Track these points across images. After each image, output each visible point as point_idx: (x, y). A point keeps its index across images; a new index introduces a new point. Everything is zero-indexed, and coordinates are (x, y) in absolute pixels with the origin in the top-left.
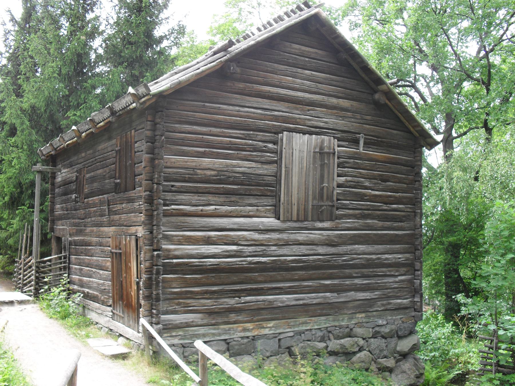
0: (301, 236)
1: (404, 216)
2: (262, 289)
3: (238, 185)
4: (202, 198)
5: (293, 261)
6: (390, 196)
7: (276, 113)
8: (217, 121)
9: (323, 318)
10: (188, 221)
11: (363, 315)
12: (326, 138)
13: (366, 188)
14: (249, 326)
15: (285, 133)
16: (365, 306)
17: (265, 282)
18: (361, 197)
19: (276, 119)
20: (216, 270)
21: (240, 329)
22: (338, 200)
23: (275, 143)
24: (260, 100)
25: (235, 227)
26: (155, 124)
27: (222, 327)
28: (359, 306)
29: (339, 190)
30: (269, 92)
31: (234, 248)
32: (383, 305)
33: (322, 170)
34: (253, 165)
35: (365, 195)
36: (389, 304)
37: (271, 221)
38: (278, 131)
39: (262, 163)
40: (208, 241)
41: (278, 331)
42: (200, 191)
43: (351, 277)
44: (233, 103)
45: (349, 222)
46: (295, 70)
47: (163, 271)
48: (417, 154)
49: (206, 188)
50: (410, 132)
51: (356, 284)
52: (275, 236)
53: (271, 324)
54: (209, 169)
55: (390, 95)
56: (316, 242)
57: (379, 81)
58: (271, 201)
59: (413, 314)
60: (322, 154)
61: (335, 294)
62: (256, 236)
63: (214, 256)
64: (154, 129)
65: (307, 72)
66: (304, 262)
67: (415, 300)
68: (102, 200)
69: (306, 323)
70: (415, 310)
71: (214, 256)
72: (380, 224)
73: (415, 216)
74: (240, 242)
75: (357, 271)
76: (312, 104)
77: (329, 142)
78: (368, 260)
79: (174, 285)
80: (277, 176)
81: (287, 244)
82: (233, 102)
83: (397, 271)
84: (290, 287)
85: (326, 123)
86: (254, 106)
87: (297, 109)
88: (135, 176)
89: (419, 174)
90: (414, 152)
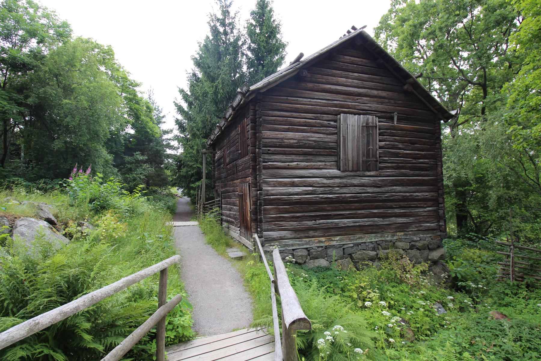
1: (429, 167)
2: (330, 215)
5: (350, 197)
7: (335, 102)
8: (296, 108)
9: (373, 235)
12: (370, 117)
13: (400, 149)
14: (323, 239)
15: (342, 114)
19: (336, 106)
20: (299, 203)
25: (311, 175)
29: (381, 151)
31: (311, 188)
32: (416, 227)
39: (327, 134)
40: (293, 185)
41: (342, 243)
45: (389, 171)
50: (431, 110)
51: (396, 213)
52: (337, 181)
53: (338, 238)
54: (292, 139)
61: (381, 219)
62: (325, 181)
65: (356, 74)
66: (358, 197)
67: (440, 224)
72: (412, 172)
73: (437, 167)
76: (360, 95)
78: (403, 196)
80: (338, 142)
81: (346, 186)
82: (306, 96)
84: (349, 214)
86: (321, 98)
87: (349, 99)
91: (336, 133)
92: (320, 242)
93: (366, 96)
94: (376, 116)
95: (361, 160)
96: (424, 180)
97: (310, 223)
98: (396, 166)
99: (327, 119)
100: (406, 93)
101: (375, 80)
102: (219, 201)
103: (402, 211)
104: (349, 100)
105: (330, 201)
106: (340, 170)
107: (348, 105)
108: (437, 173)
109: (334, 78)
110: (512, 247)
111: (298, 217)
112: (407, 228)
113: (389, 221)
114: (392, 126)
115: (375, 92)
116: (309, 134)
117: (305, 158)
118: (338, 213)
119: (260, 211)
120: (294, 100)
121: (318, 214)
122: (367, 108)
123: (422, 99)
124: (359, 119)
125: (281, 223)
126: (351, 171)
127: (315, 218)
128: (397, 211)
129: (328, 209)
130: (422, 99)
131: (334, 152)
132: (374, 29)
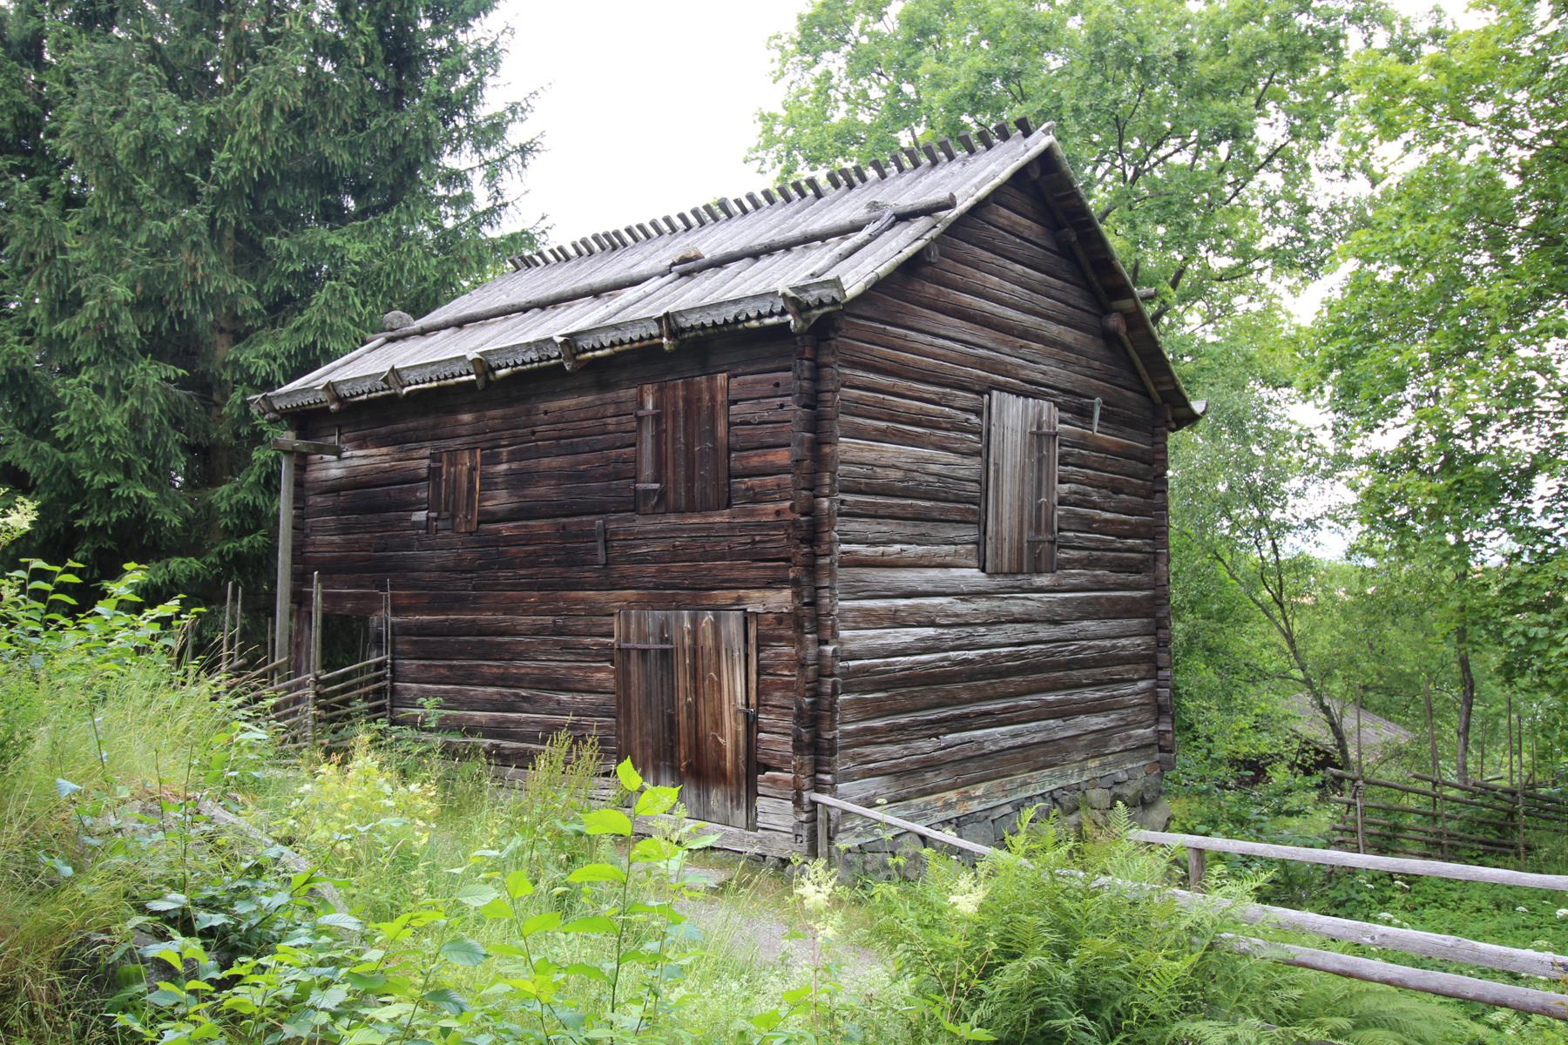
0: (1016, 606)
1: (1142, 562)
2: (966, 716)
3: (930, 500)
4: (884, 529)
5: (1009, 656)
6: (1125, 522)
7: (981, 352)
8: (903, 364)
9: (1047, 772)
10: (863, 577)
11: (1096, 763)
12: (1045, 404)
13: (1094, 506)
14: (952, 796)
15: (995, 393)
16: (1097, 744)
17: (971, 701)
18: (1088, 525)
19: (981, 363)
20: (911, 679)
21: (940, 804)
22: (1060, 530)
23: (978, 413)
24: (957, 322)
25: (929, 587)
26: (818, 367)
27: (914, 801)
28: (1089, 746)
29: (1060, 511)
30: (970, 306)
31: (931, 631)
32: (1122, 741)
33: (1040, 470)
34: (951, 457)
35: (1093, 520)
36: (1129, 737)
37: (972, 576)
38: (986, 389)
39: (963, 454)
40: (896, 620)
41: (990, 805)
42: (881, 512)
43: (1079, 686)
44: (923, 327)
45: (1077, 575)
46: (1002, 261)
47: (843, 686)
48: (1158, 439)
49: (889, 506)
50: (1147, 395)
51: (1085, 701)
52: (983, 604)
53: (980, 790)
54: (894, 466)
55: (1136, 321)
56: (1035, 617)
57: (1123, 291)
58: (970, 533)
59: (1158, 756)
60: (1039, 437)
61: (1060, 722)
62: (961, 607)
63: (904, 652)
64: (816, 378)
65: (1018, 267)
66: (1022, 657)
67: (1161, 728)
68: (327, 541)
69: (1024, 784)
70: (1161, 749)
71: (904, 652)
72: (1113, 577)
73: (1155, 560)
74: (938, 620)
75: (1087, 672)
76: (1025, 334)
77: (1048, 411)
78: (1102, 649)
79: (849, 717)
80: (983, 482)
81: (995, 621)
82: (923, 325)
83: (1136, 671)
84: (1004, 710)
85: (1044, 373)
86: (952, 334)
87: (1005, 343)
88: (730, 477)
89: (1161, 479)
90: (1153, 435)
91: (978, 453)
92: (948, 805)
93: (1038, 338)
94: (1056, 404)
95: (1026, 538)
96: (1134, 598)
97: (927, 745)
98: (1087, 558)
99: (965, 404)
100: (1109, 338)
101: (1053, 292)
102: (379, 666)
103: (1098, 694)
104: (1007, 350)
105: (969, 673)
106: (983, 570)
107: (1003, 363)
108: (1156, 579)
109: (979, 274)
110: (1360, 783)
111: (903, 727)
112: (1105, 746)
113: (1075, 726)
114: (1083, 436)
115: (1054, 330)
116: (926, 452)
117: (917, 531)
118: (983, 708)
119: (832, 710)
120: (898, 337)
121: (933, 715)
122: (1038, 377)
123: (1137, 360)
124: (1026, 407)
125: (867, 750)
126: (1006, 574)
127: (935, 728)
128: (1090, 694)
129: (965, 696)
130: (1137, 360)
131: (974, 512)
132: (800, 18)
